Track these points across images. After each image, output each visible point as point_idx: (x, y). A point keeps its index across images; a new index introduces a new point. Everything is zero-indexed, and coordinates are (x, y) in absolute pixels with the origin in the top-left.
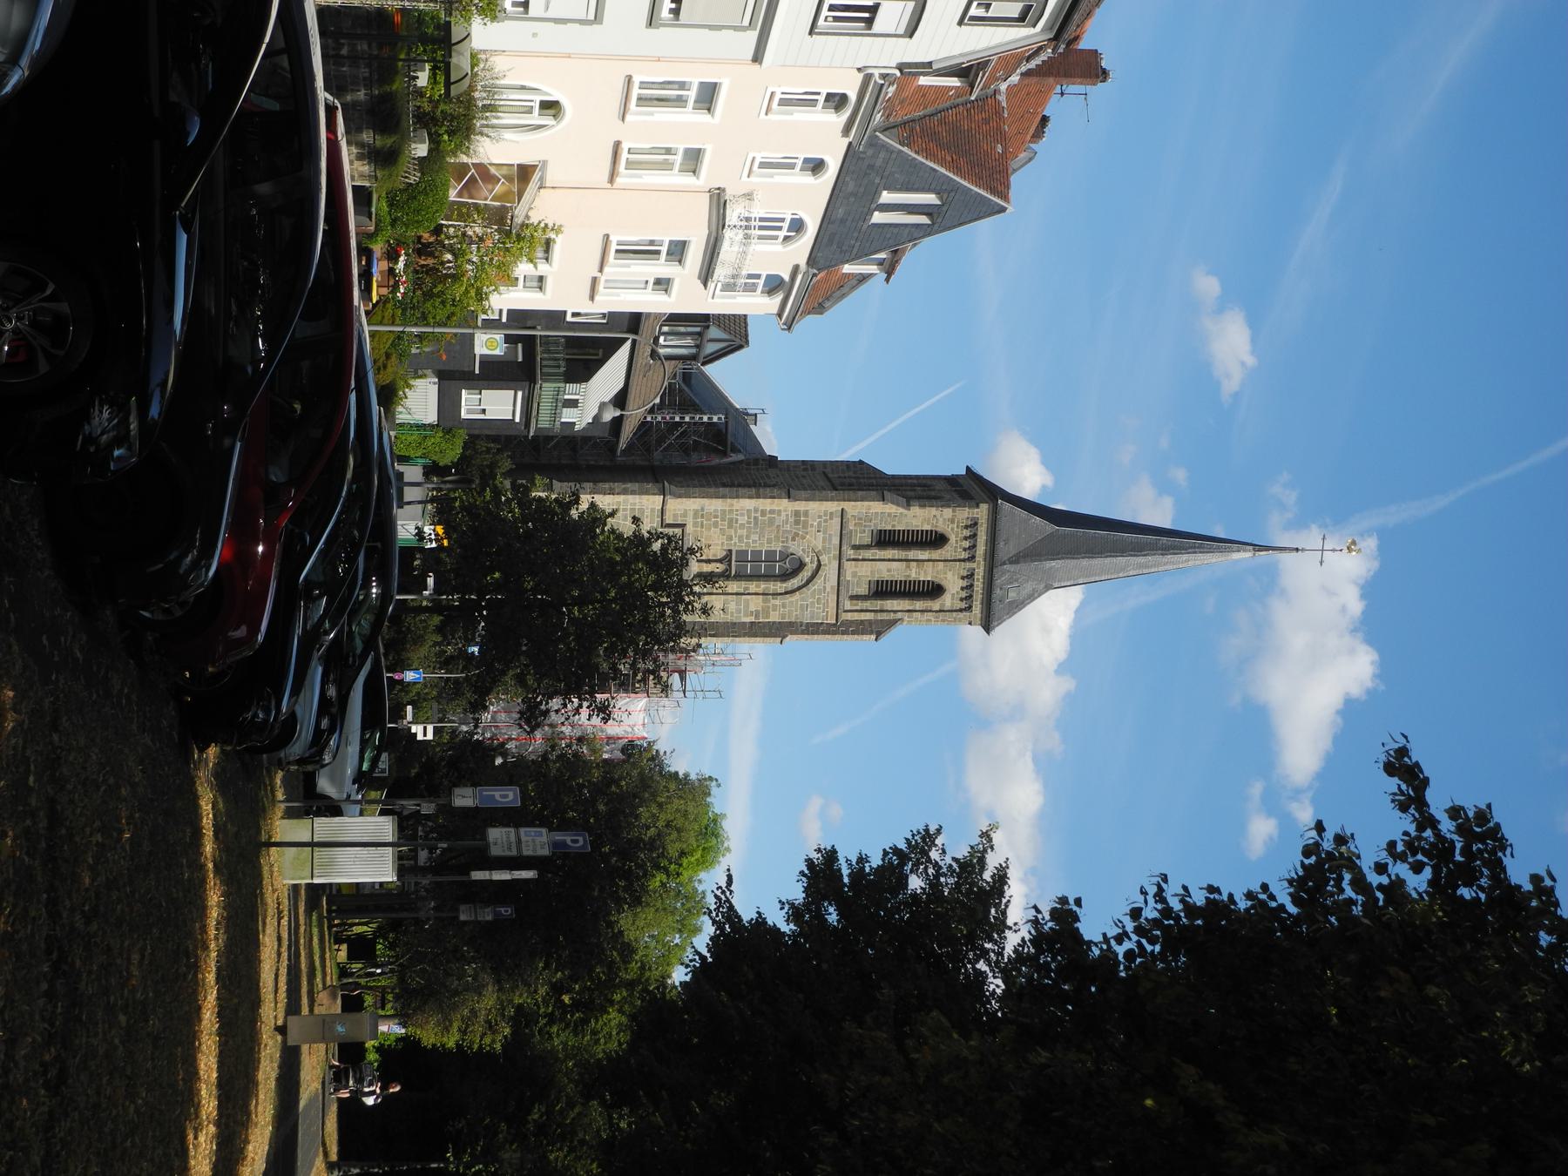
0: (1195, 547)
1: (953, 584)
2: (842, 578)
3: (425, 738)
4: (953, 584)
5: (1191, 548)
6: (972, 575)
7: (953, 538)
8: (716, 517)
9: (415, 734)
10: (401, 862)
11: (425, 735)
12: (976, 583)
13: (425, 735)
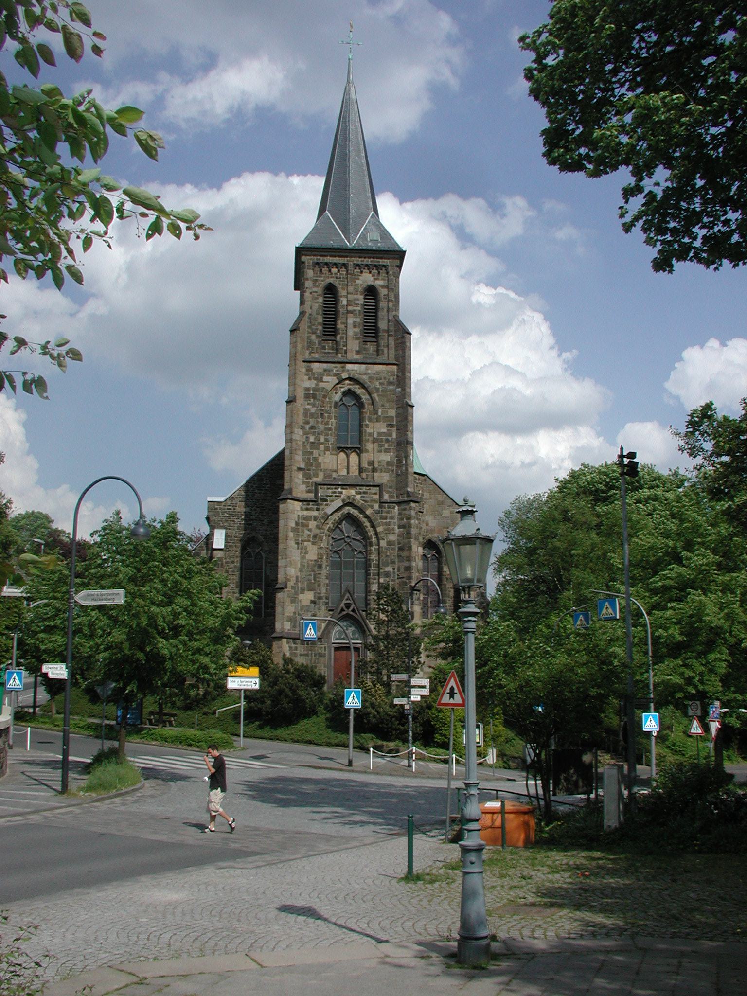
0: (345, 122)
1: (367, 278)
2: (360, 361)
3: (428, 687)
4: (367, 278)
5: (346, 124)
6: (358, 265)
7: (331, 280)
8: (309, 459)
9: (422, 697)
10: (352, 711)
11: (424, 687)
12: (365, 263)
13: (424, 687)
